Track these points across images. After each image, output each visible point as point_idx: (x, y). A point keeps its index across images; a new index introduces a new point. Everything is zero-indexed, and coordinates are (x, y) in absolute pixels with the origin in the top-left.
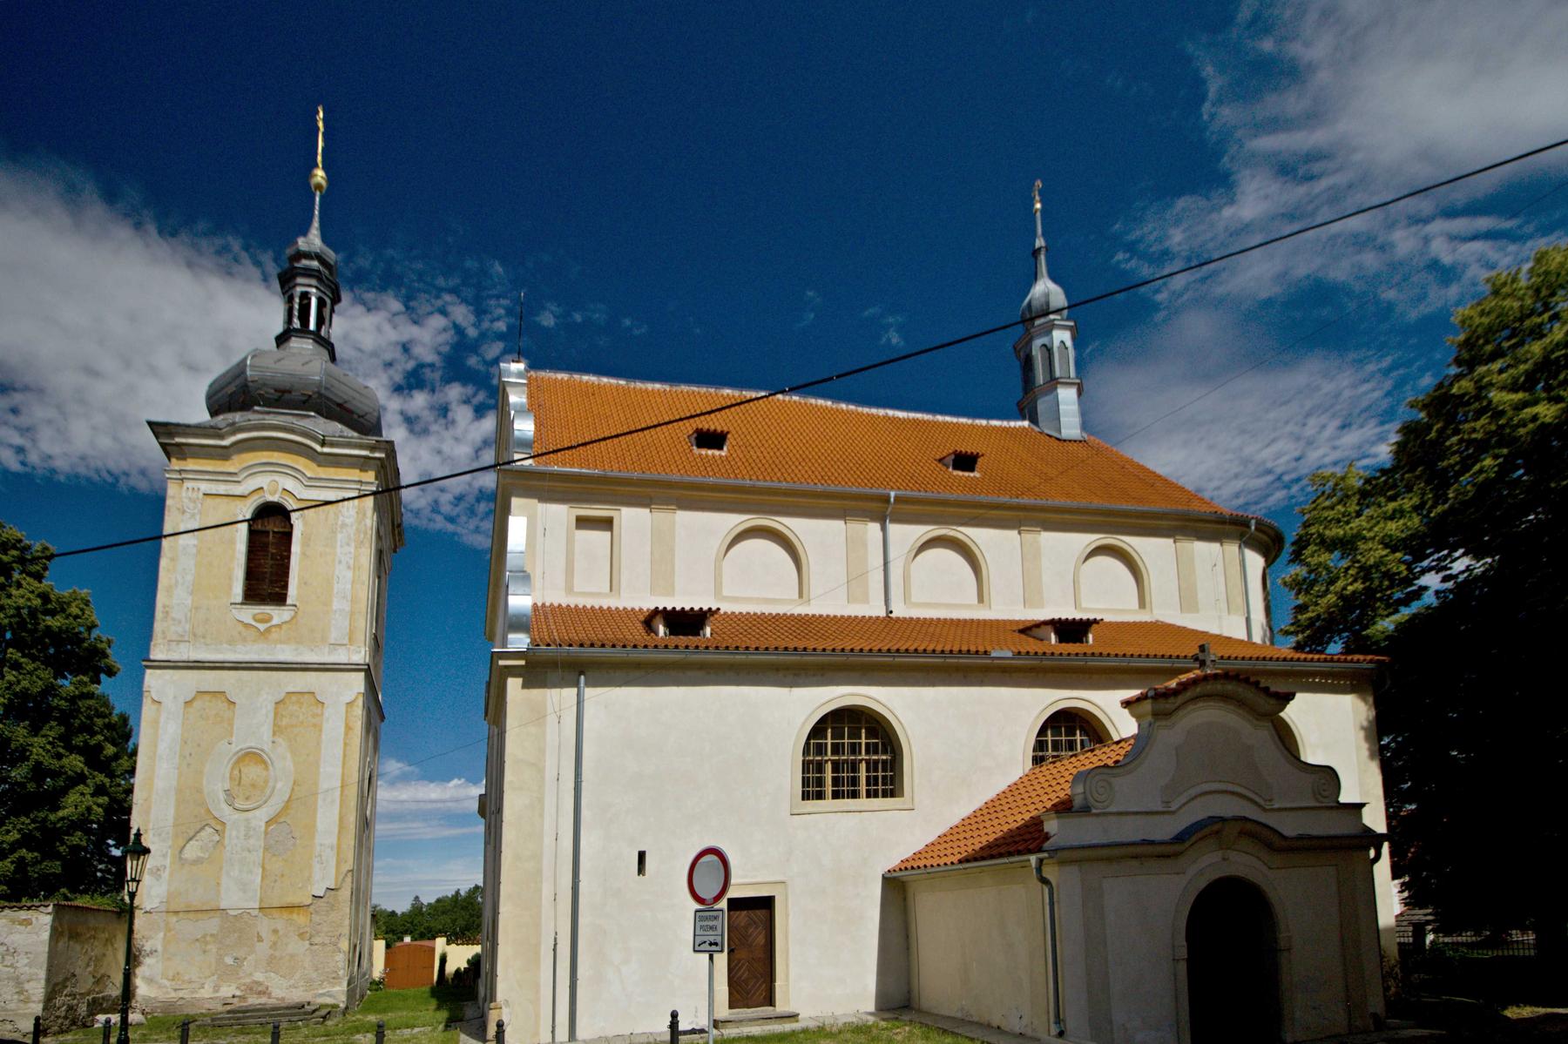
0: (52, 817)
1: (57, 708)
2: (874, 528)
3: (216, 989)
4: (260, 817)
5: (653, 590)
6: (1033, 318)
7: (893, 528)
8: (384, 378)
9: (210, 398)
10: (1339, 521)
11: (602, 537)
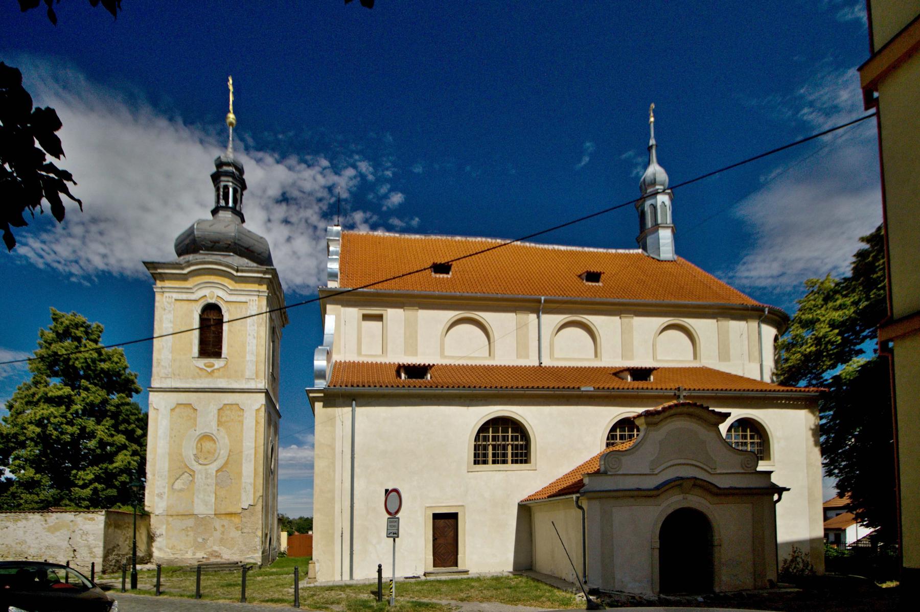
0: (110, 467)
1: (109, 410)
2: (533, 317)
3: (194, 554)
4: (213, 468)
5: (406, 353)
6: (645, 191)
7: (544, 317)
8: (316, 208)
9: (176, 246)
10: (811, 309)
11: (378, 324)
